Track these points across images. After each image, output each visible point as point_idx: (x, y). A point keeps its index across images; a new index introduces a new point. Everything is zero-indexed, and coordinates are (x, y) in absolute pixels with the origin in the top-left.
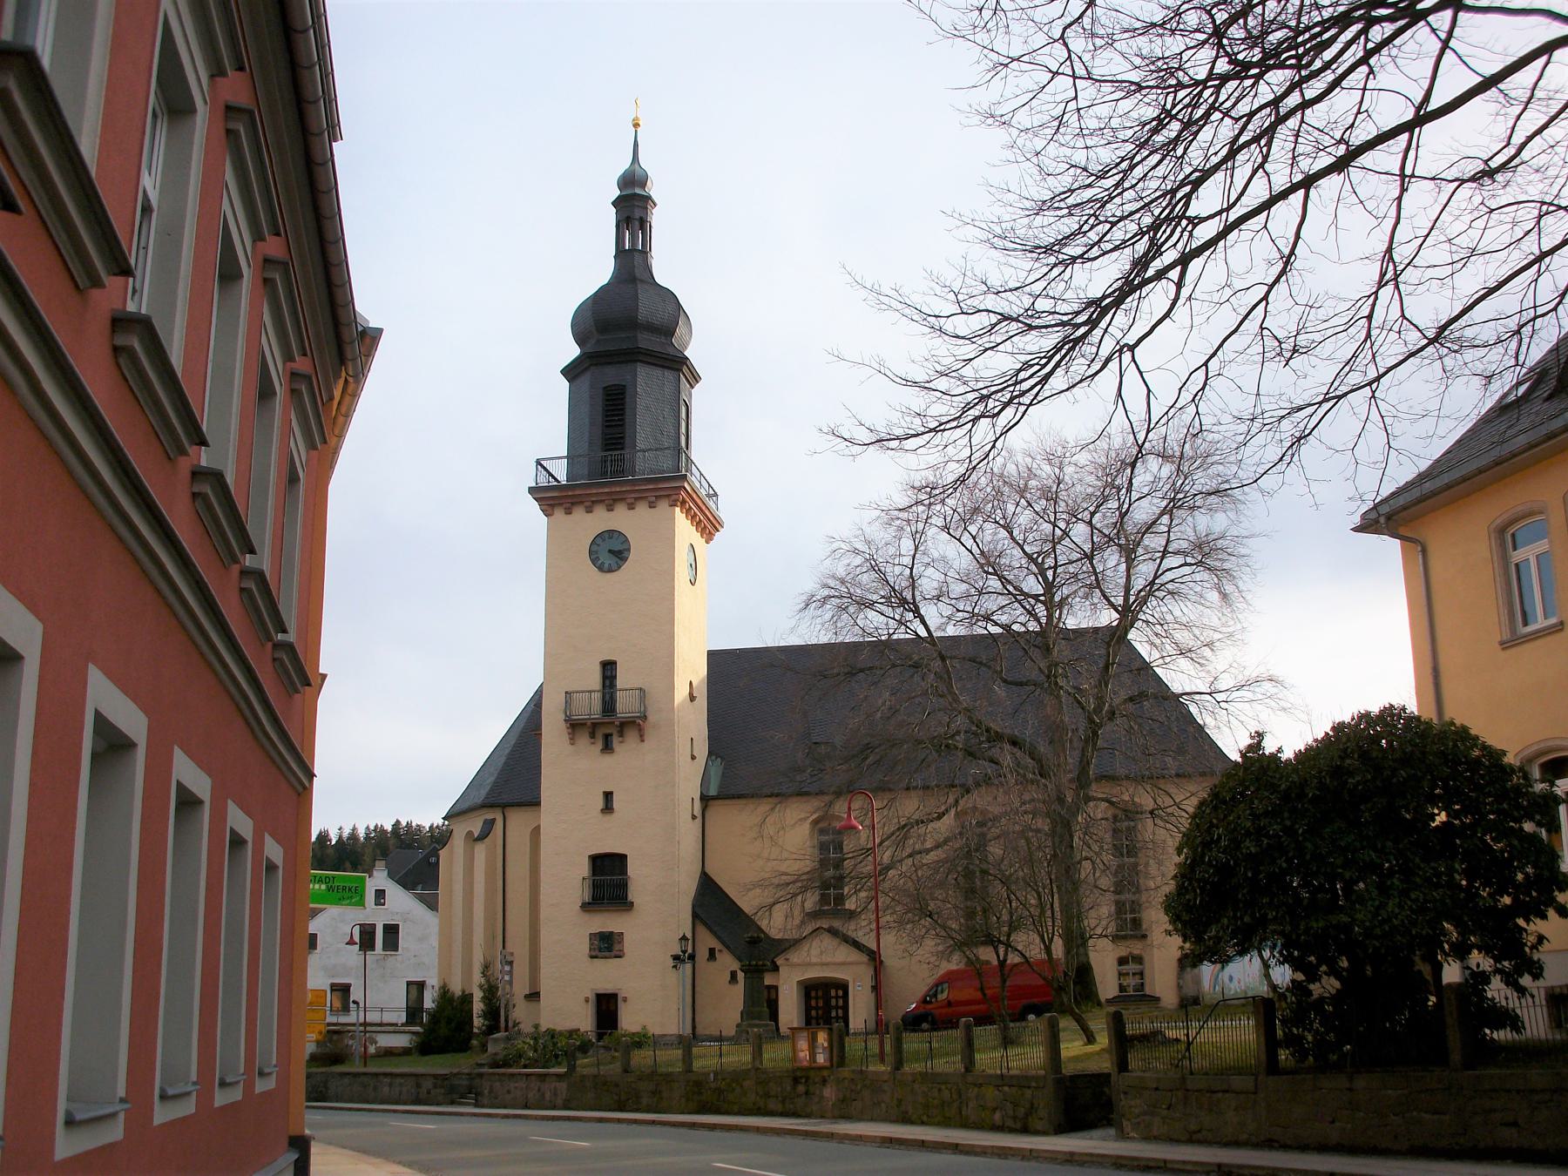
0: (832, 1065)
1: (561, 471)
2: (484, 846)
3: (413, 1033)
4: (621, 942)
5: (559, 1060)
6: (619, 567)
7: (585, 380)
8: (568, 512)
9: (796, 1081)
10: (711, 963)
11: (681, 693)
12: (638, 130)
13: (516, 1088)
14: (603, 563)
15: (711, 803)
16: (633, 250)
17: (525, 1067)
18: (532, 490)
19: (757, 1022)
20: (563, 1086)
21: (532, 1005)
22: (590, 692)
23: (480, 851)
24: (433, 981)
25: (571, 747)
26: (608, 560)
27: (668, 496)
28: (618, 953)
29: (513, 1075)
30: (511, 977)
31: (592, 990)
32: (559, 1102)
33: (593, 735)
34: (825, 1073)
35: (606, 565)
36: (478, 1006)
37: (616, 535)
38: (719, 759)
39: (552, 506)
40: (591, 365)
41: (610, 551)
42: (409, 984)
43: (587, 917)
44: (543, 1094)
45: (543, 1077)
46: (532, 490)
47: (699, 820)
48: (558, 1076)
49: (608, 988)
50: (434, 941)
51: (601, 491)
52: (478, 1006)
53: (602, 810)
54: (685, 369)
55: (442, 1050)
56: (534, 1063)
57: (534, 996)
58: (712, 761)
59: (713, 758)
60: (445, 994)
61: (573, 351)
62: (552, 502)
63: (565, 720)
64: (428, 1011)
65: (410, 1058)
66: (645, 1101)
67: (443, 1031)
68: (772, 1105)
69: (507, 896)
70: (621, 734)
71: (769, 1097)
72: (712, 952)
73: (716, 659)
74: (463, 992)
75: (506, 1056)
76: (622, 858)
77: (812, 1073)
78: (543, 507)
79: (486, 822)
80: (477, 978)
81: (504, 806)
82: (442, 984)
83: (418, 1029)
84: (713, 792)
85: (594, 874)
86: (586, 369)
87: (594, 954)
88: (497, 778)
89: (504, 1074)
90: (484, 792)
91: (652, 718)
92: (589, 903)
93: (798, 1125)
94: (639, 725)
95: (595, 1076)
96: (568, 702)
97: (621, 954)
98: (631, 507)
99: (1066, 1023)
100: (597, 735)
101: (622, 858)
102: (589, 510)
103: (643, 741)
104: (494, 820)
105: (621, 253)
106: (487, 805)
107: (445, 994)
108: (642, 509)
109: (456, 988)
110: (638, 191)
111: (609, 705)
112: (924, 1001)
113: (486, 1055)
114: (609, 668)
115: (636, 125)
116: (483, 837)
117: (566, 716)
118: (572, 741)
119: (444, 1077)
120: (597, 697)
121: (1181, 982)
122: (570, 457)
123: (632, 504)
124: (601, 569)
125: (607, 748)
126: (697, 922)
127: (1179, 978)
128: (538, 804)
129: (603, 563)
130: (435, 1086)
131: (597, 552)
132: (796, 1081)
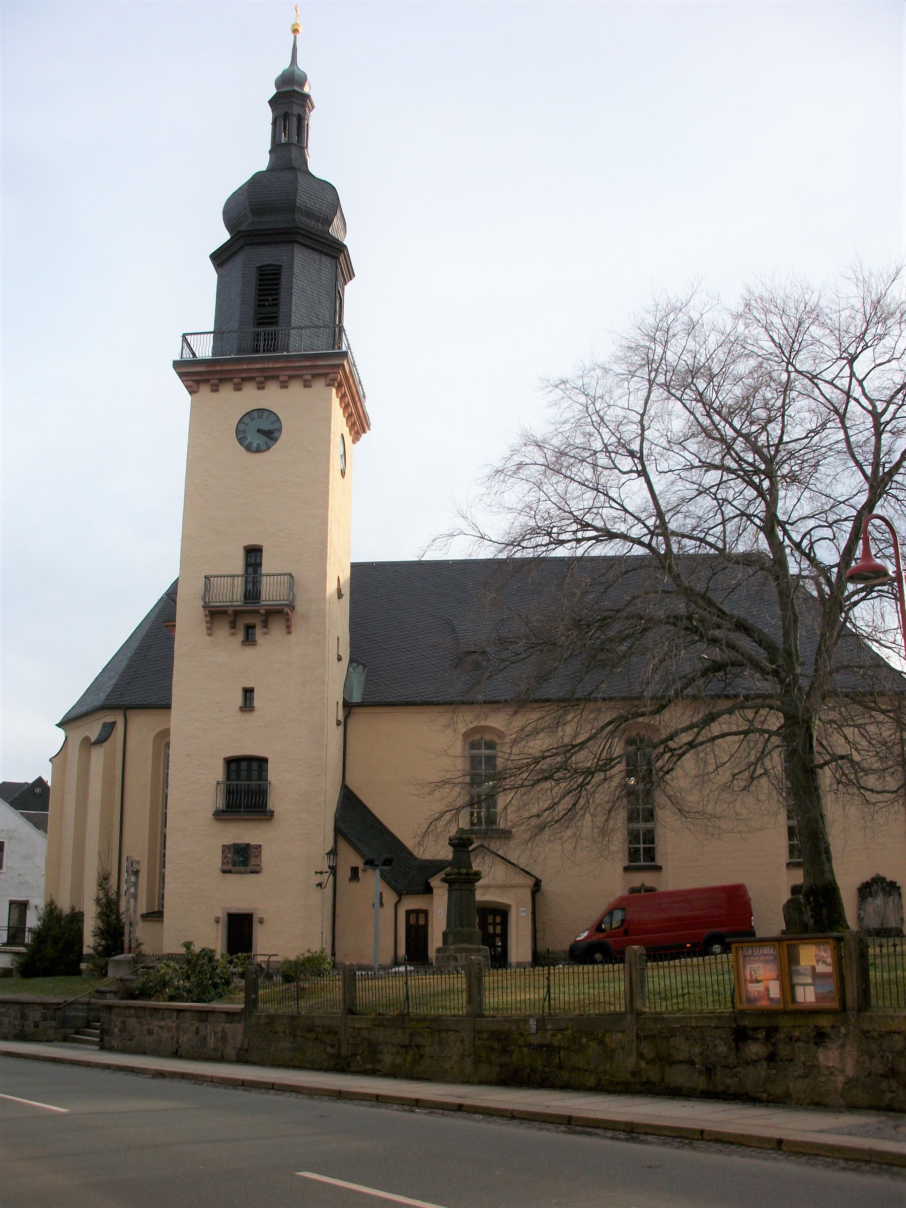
0: (844, 1008)
1: (204, 349)
2: (103, 749)
3: (17, 954)
4: (258, 856)
5: (220, 990)
6: (268, 448)
7: (237, 264)
8: (215, 389)
9: (741, 1035)
10: (354, 885)
11: (331, 588)
12: (298, 36)
13: (161, 1027)
14: (251, 444)
15: (354, 710)
16: (288, 145)
17: (172, 998)
18: (177, 365)
19: (466, 945)
20: (236, 1030)
21: (155, 926)
22: (233, 576)
23: (98, 756)
24: (38, 902)
25: (209, 638)
26: (257, 440)
27: (325, 375)
28: (253, 868)
29: (156, 1010)
30: (136, 889)
31: (223, 908)
32: (231, 1052)
33: (233, 625)
34: (824, 1022)
35: (254, 445)
36: (90, 925)
37: (266, 414)
38: (361, 667)
39: (198, 382)
40: (246, 244)
41: (259, 431)
42: (12, 903)
43: (220, 827)
44: (205, 1038)
45: (204, 1015)
46: (177, 365)
47: (341, 727)
48: (230, 1015)
49: (240, 906)
50: (40, 861)
51: (252, 366)
52: (90, 925)
53: (241, 707)
54: (342, 258)
55: (47, 972)
56: (190, 995)
57: (155, 915)
58: (354, 668)
59: (355, 665)
60: (51, 913)
61: (224, 236)
62: (198, 378)
63: (203, 607)
64: (30, 930)
65: (9, 980)
66: (387, 1059)
67: (49, 951)
68: (678, 1076)
69: (126, 806)
70: (265, 624)
71: (672, 1063)
72: (355, 871)
73: (357, 569)
74: (73, 909)
75: (144, 984)
76: (262, 762)
77: (784, 1023)
78: (190, 383)
79: (105, 725)
80: (91, 890)
81: (126, 709)
82: (49, 900)
83: (23, 949)
84: (356, 698)
85: (228, 778)
86: (241, 248)
87: (227, 868)
88: (119, 680)
89: (144, 1008)
90: (102, 696)
91: (300, 607)
92: (223, 811)
93: (838, 1131)
94: (287, 614)
95: (293, 1018)
96: (207, 588)
97: (257, 869)
98: (284, 385)
99: (552, 968)
100: (237, 626)
101: (262, 762)
102: (238, 388)
103: (289, 633)
104: (113, 724)
105: (276, 147)
106: (105, 707)
107: (51, 912)
108: (296, 388)
109: (65, 906)
110: (297, 89)
111: (252, 593)
112: (598, 929)
113: (105, 979)
114: (253, 554)
115: (295, 31)
116: (101, 741)
117: (205, 603)
118: (210, 632)
119: (57, 1007)
120: (239, 582)
121: (862, 913)
122: (218, 333)
123: (286, 382)
124: (248, 448)
125: (249, 640)
126: (340, 839)
127: (860, 909)
128: (168, 707)
129: (251, 444)
130: (45, 1019)
131: (244, 431)
132: (741, 1035)
